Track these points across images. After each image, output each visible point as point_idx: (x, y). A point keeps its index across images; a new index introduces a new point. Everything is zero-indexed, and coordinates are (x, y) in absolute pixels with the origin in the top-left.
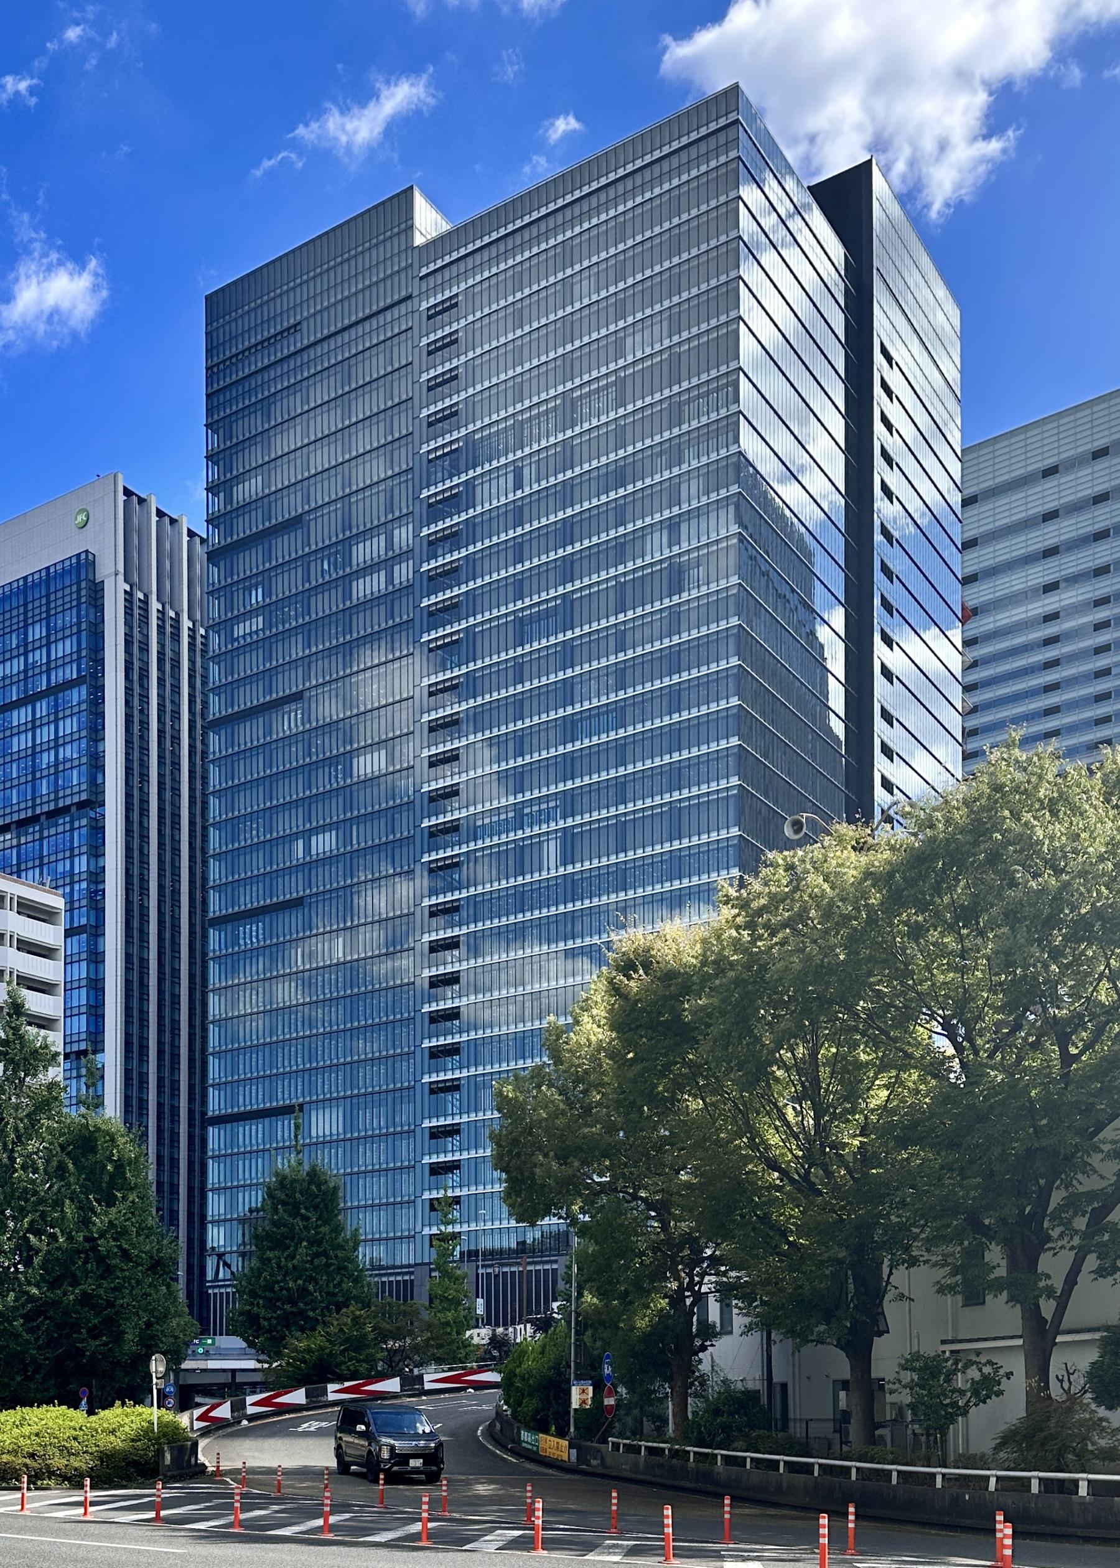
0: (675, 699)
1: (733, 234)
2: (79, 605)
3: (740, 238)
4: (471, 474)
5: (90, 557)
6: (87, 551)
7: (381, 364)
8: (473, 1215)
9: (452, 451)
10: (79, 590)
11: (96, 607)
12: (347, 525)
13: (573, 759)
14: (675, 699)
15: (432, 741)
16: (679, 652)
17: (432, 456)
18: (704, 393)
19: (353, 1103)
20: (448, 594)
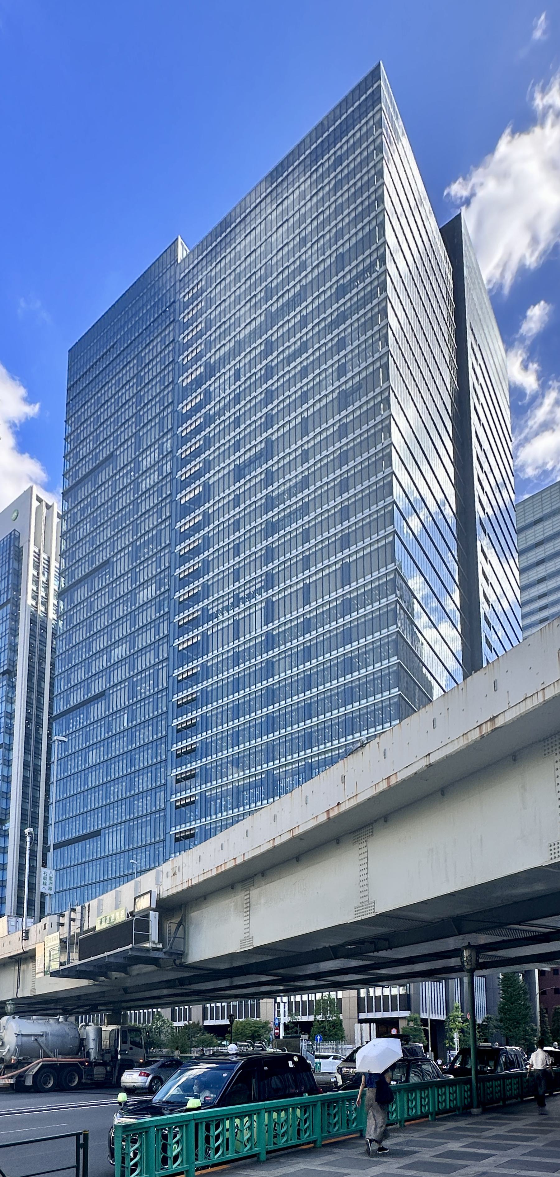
0: (349, 695)
1: (389, 500)
2: (9, 562)
3: (394, 502)
4: (207, 530)
5: (17, 533)
6: (15, 530)
7: (153, 635)
8: (207, 464)
9: (193, 675)
10: (9, 554)
11: (7, 782)
12: (131, 829)
13: (273, 746)
14: (349, 695)
15: (177, 849)
16: (353, 718)
17: (180, 678)
18: (369, 562)
19: (128, 825)
20: (190, 741)
